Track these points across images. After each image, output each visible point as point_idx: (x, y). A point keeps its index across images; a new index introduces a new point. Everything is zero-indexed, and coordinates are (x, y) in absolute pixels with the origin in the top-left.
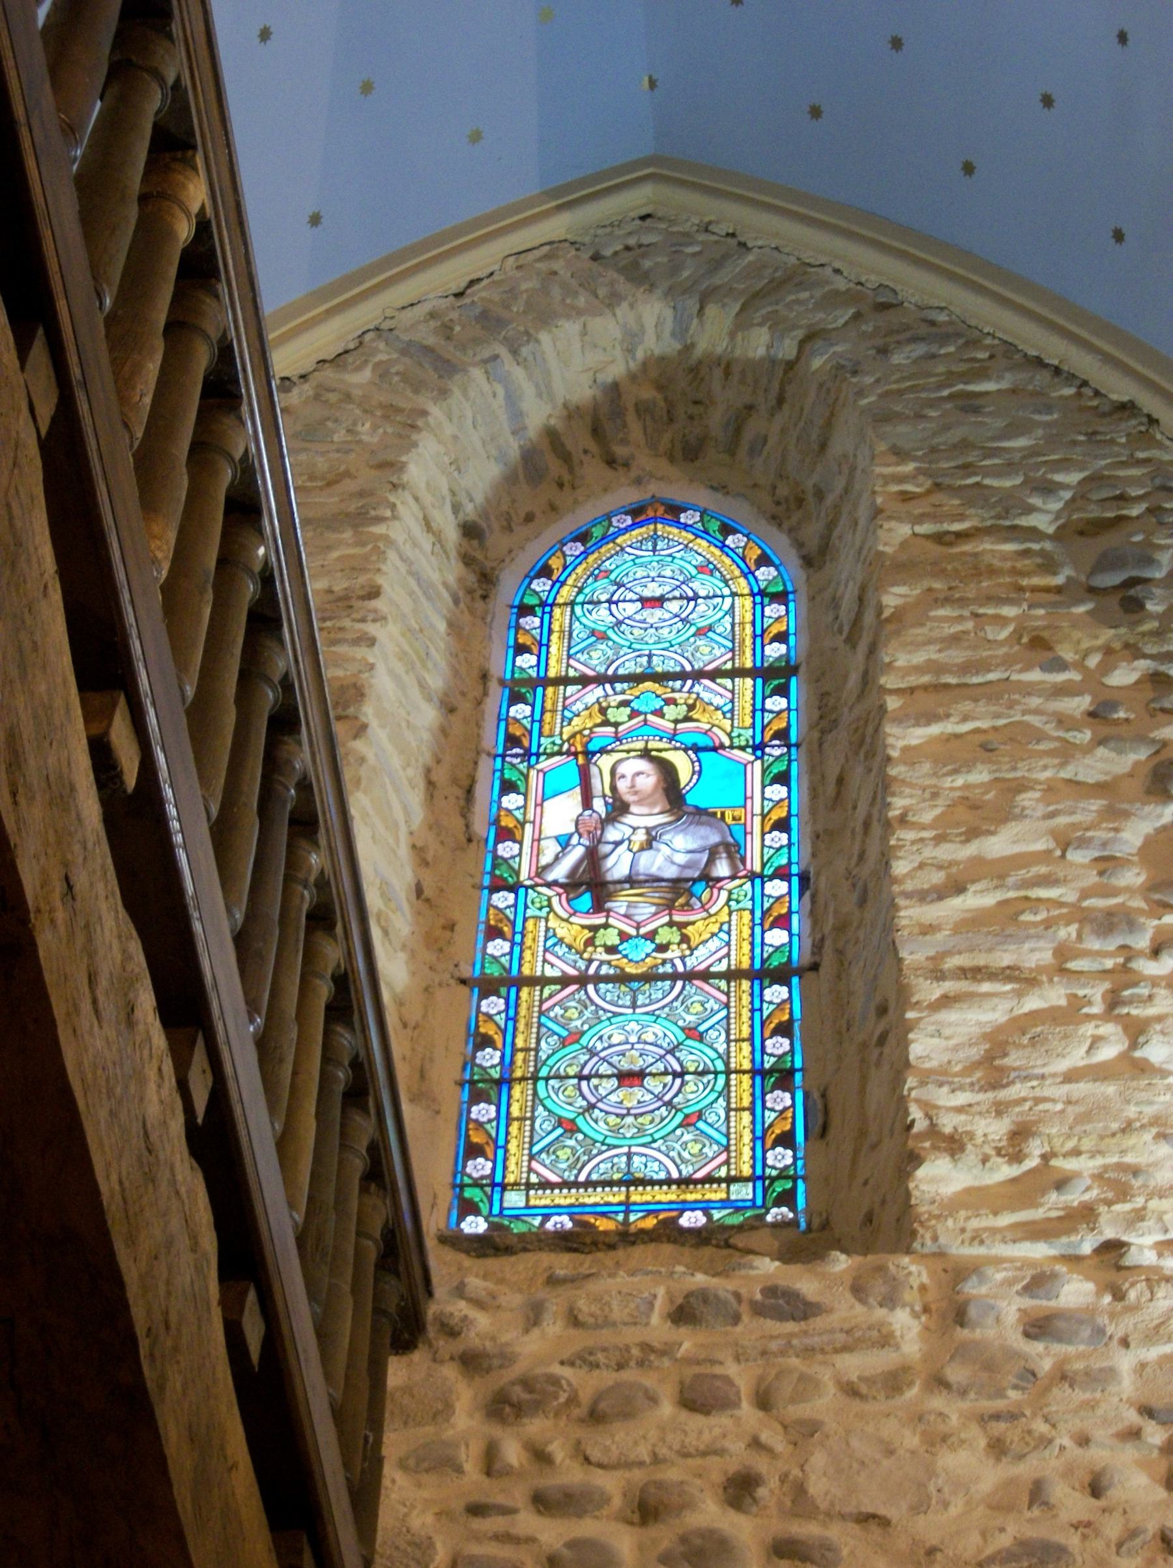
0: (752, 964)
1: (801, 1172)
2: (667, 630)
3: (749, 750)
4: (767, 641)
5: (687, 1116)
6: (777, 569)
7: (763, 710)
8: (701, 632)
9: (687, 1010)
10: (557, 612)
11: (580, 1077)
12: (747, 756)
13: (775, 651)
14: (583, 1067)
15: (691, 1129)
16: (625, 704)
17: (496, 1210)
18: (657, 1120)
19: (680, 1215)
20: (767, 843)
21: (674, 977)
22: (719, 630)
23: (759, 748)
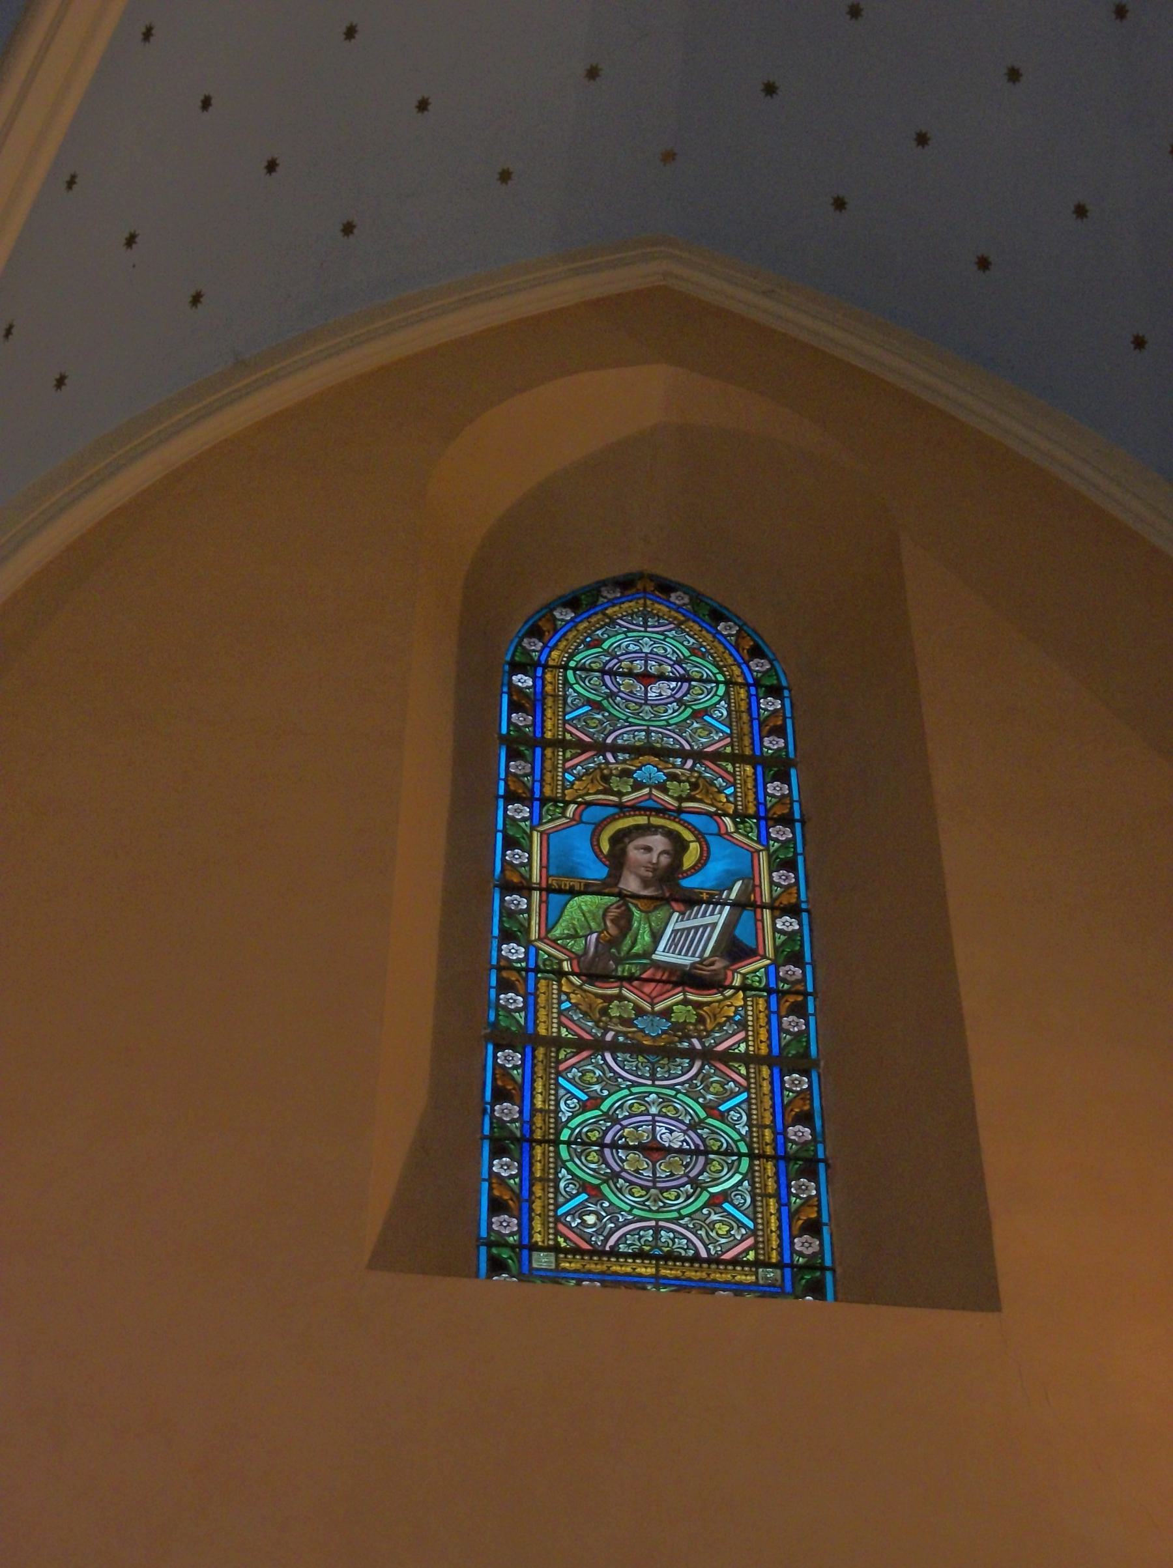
0: (770, 1051)
1: (810, 989)
2: (673, 1193)
5: (695, 712)
6: (771, 662)
8: (697, 715)
9: (706, 1089)
11: (603, 672)
13: (773, 744)
14: (606, 1132)
15: (718, 1210)
16: (627, 773)
18: (670, 711)
22: (738, 1200)
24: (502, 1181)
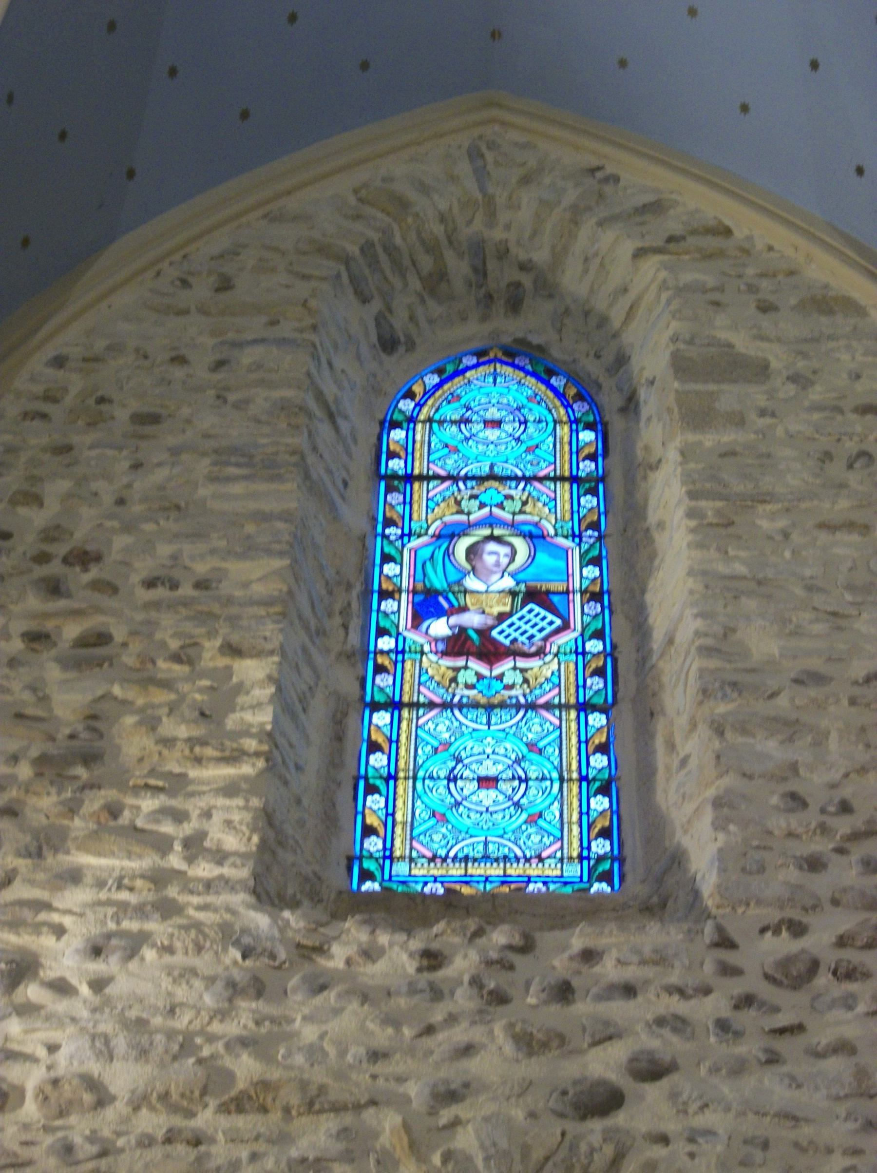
3: (571, 538)
4: (581, 458)
5: (529, 816)
7: (584, 653)
10: (419, 427)
12: (568, 543)
13: (587, 467)
17: (386, 877)
19: (527, 886)
20: (586, 610)
21: (518, 707)
23: (576, 536)
24: (392, 507)
